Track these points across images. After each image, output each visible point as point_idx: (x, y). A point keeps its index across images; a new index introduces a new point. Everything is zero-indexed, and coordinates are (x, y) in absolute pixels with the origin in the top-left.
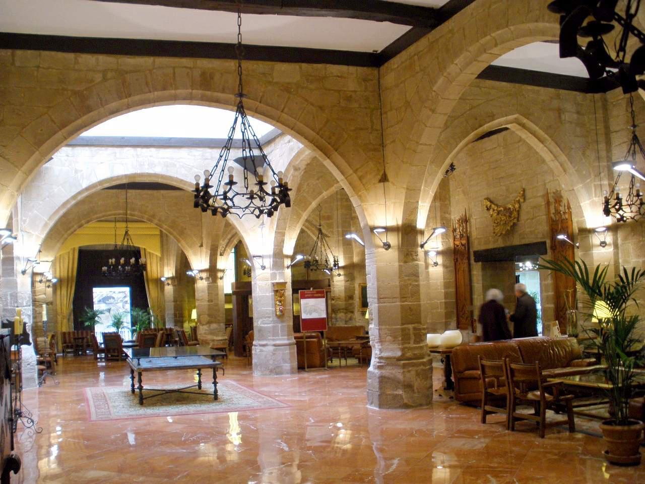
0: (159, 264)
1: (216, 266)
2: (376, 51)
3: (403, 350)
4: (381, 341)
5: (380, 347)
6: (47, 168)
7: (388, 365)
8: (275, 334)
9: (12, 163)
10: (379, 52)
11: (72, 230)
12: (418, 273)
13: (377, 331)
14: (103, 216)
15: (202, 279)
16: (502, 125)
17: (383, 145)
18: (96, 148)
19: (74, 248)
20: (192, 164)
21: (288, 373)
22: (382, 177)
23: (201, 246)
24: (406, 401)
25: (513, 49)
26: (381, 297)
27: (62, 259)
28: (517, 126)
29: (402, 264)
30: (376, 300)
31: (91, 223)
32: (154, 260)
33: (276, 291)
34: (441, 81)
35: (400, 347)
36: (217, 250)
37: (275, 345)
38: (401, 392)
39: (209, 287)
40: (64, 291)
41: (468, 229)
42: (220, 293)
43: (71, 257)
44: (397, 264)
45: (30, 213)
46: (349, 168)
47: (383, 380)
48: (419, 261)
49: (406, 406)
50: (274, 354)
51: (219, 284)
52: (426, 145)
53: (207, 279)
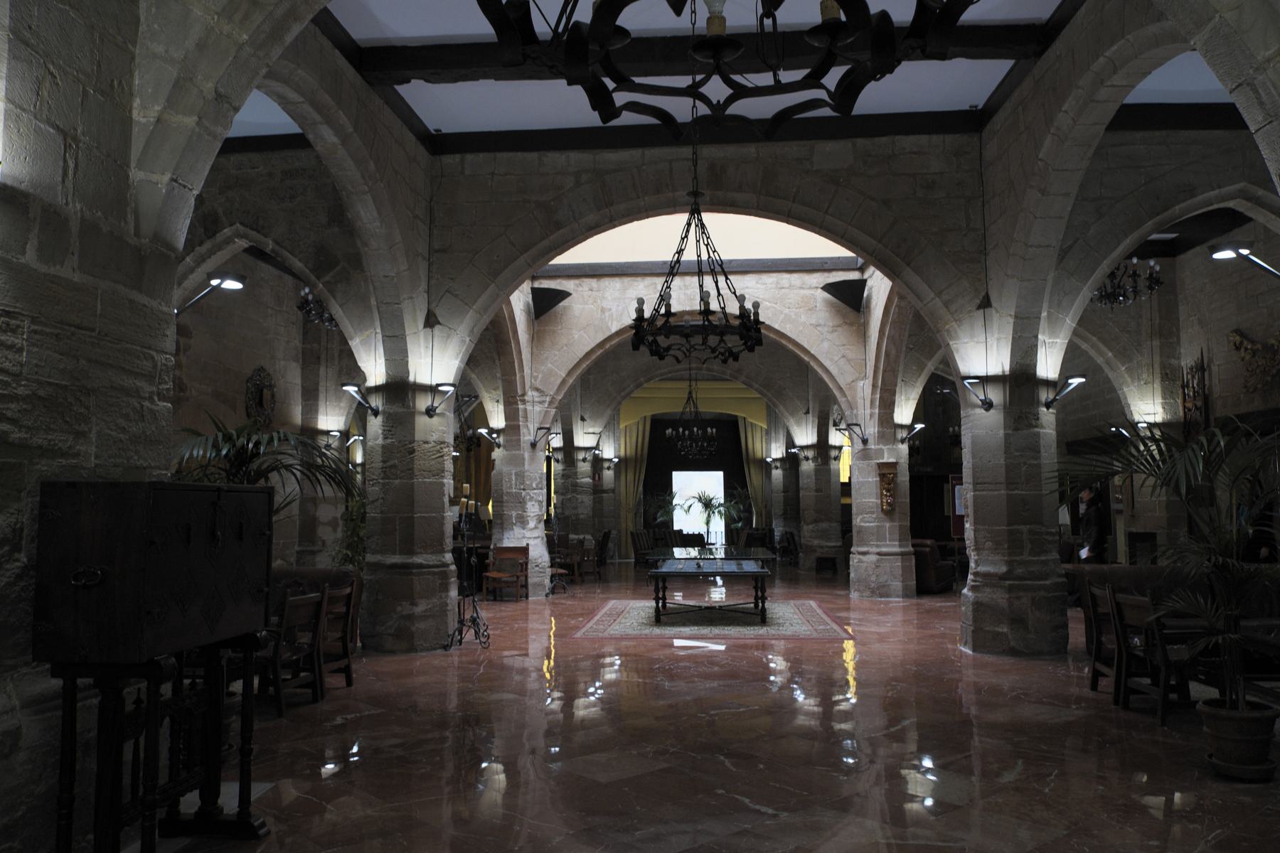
0: (764, 440)
1: (828, 441)
2: (976, 107)
3: (1009, 563)
4: (977, 549)
5: (976, 557)
6: (565, 308)
7: (986, 585)
8: (880, 537)
9: (462, 300)
10: (980, 107)
11: (627, 391)
12: (1039, 446)
13: (972, 533)
14: (670, 373)
15: (807, 459)
16: (1212, 204)
17: (984, 252)
18: (629, 279)
19: (645, 417)
20: (761, 297)
21: (898, 596)
22: (982, 302)
23: (807, 412)
24: (1013, 643)
25: (1150, 73)
26: (979, 481)
27: (628, 430)
28: (1244, 202)
29: (1010, 432)
30: (971, 486)
31: (652, 381)
32: (758, 435)
33: (882, 476)
34: (1048, 141)
35: (1006, 558)
36: (828, 419)
37: (879, 554)
38: (1005, 630)
39: (817, 471)
40: (630, 476)
41: (1206, 382)
42: (833, 479)
43: (641, 428)
44: (1001, 432)
45: (543, 368)
46: (930, 290)
47: (978, 606)
48: (1042, 427)
49: (1013, 652)
50: (877, 567)
51: (832, 467)
52: (1039, 246)
53: (815, 459)
